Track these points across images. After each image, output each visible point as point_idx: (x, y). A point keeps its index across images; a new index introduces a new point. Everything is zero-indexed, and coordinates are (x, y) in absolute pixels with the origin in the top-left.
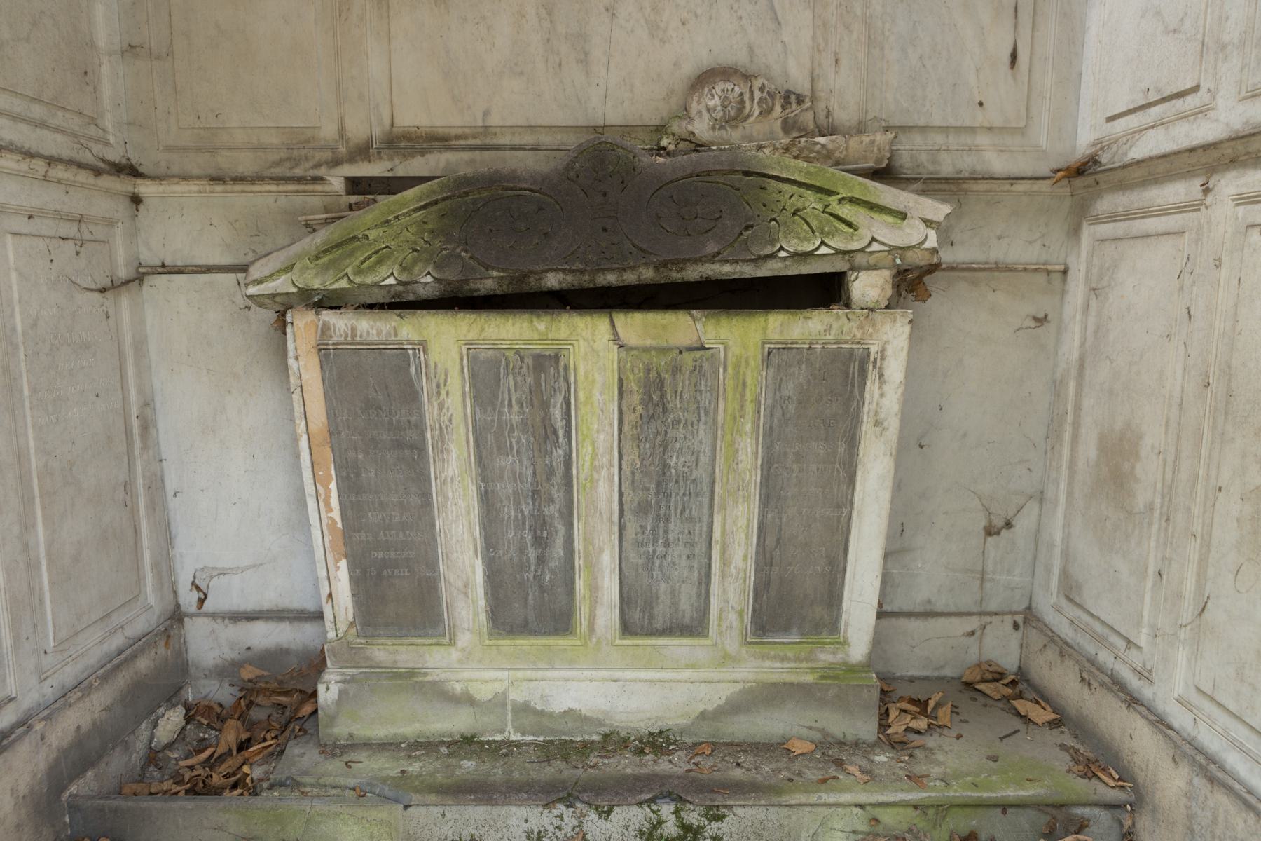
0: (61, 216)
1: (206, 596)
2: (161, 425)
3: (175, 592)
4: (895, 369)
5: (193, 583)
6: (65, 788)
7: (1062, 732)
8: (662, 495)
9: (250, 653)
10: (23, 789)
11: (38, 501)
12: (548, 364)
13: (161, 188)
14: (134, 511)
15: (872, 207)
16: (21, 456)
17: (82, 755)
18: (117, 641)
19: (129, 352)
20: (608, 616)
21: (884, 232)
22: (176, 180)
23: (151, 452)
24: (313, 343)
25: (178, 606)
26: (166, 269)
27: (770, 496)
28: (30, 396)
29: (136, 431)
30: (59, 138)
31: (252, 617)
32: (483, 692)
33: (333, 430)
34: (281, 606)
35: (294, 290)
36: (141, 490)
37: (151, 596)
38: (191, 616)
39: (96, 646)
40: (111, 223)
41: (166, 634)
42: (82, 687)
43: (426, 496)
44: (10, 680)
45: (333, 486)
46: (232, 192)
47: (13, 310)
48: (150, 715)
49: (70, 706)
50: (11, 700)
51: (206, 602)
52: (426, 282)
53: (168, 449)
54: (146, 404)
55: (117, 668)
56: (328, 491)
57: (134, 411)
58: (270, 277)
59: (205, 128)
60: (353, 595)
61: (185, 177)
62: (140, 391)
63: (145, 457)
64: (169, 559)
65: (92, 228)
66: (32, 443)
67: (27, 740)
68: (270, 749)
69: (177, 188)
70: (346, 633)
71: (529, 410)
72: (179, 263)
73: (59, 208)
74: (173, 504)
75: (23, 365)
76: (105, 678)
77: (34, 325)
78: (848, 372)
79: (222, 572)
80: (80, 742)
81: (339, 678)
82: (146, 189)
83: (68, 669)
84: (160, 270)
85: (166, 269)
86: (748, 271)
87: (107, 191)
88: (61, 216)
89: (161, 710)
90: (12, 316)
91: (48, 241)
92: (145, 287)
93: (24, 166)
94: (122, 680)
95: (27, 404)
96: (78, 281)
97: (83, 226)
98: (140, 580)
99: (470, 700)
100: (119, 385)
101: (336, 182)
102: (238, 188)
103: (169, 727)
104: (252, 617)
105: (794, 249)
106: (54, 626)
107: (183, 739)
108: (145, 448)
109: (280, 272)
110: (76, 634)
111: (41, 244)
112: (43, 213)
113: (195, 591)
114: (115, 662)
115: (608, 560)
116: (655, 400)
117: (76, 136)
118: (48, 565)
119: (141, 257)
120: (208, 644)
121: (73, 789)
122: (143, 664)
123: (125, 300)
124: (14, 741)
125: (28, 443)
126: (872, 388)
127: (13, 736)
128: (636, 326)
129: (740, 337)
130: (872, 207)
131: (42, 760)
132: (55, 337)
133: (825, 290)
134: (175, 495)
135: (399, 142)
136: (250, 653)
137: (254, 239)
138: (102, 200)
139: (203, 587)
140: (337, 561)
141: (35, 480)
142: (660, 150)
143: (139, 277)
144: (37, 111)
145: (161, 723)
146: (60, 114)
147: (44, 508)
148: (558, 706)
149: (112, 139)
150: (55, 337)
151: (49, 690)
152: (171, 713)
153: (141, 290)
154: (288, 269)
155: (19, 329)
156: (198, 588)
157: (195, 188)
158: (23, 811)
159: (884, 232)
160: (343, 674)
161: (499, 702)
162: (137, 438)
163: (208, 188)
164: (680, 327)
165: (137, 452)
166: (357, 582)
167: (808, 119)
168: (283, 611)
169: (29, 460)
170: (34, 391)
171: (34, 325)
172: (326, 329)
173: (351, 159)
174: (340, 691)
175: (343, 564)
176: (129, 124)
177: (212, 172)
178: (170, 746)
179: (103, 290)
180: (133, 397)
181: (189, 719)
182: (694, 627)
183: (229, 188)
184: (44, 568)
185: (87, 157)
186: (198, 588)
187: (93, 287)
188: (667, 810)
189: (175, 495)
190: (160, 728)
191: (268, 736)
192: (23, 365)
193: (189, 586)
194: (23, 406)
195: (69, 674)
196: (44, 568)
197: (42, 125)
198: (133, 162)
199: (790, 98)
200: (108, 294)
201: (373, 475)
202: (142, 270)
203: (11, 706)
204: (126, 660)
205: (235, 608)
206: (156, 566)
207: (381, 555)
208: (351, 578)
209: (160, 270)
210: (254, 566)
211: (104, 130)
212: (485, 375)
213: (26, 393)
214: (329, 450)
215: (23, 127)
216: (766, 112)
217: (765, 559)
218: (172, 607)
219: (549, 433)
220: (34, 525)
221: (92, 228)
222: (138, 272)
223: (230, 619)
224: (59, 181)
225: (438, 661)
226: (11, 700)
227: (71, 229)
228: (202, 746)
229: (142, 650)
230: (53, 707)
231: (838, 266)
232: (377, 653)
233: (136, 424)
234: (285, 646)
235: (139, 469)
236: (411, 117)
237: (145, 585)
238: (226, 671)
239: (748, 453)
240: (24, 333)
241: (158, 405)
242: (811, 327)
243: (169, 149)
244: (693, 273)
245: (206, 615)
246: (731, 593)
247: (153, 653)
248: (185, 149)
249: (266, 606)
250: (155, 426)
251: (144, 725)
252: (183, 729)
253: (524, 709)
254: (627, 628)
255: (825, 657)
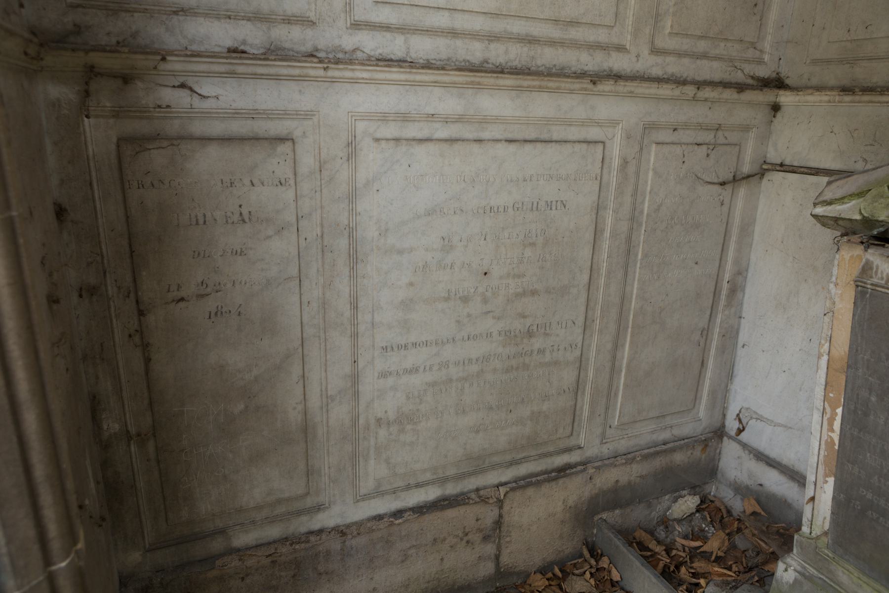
0: (701, 127)
1: (744, 429)
2: (747, 291)
3: (724, 416)
5: (738, 415)
6: (598, 513)
9: (760, 488)
10: (571, 502)
11: (630, 330)
13: (797, 98)
14: (705, 350)
16: (624, 298)
17: (615, 498)
18: (666, 435)
19: (735, 231)
22: (810, 91)
23: (733, 310)
24: (854, 276)
25: (723, 426)
26: (783, 167)
28: (642, 259)
29: (724, 292)
30: (716, 64)
31: (772, 463)
33: (852, 363)
34: (797, 468)
35: (858, 217)
36: (716, 336)
37: (702, 411)
38: (730, 437)
39: (646, 434)
40: (746, 129)
41: (705, 443)
42: (628, 457)
44: (582, 436)
45: (839, 411)
46: (859, 102)
47: (645, 198)
48: (676, 491)
49: (615, 466)
50: (580, 448)
51: (743, 434)
53: (748, 311)
54: (739, 273)
55: (657, 453)
56: (834, 414)
57: (727, 277)
58: (841, 200)
59: (851, 41)
60: (832, 513)
61: (819, 88)
62: (737, 262)
63: (727, 312)
64: (727, 390)
65: (726, 134)
66: (635, 292)
67: (581, 475)
68: (730, 579)
69: (810, 98)
70: (818, 538)
72: (796, 164)
73: (701, 120)
74: (740, 352)
75: (642, 237)
76: (646, 457)
77: (658, 210)
79: (760, 418)
80: (616, 489)
81: (799, 568)
82: (785, 98)
83: (623, 442)
84: (778, 168)
85: (783, 167)
87: (750, 104)
88: (701, 127)
89: (685, 492)
90: (643, 202)
91: (684, 147)
92: (765, 181)
93: (677, 92)
94: (658, 463)
95: (638, 265)
96: (703, 177)
97: (720, 133)
98: (696, 399)
100: (718, 257)
102: (866, 98)
103: (683, 507)
104: (772, 463)
106: (620, 413)
107: (691, 521)
108: (729, 305)
109: (852, 196)
110: (635, 422)
111: (678, 150)
112: (686, 126)
113: (737, 422)
114: (658, 449)
117: (731, 60)
118: (626, 373)
119: (768, 155)
120: (734, 464)
121: (604, 516)
122: (679, 458)
123: (742, 191)
124: (573, 474)
125: (632, 291)
127: (574, 470)
131: (587, 491)
132: (672, 219)
134: (743, 346)
136: (760, 488)
137: (869, 148)
138: (746, 110)
139: (744, 421)
140: (826, 476)
141: (631, 317)
143: (762, 171)
144: (702, 46)
145: (680, 501)
146: (722, 44)
147: (632, 336)
149: (766, 58)
150: (672, 219)
151: (606, 450)
152: (690, 498)
153: (760, 183)
154: (860, 194)
155: (646, 212)
156: (740, 421)
157: (826, 98)
158: (568, 515)
160: (804, 568)
162: (723, 297)
163: (837, 98)
165: (721, 308)
166: (840, 504)
168: (797, 473)
169: (631, 302)
170: (645, 256)
171: (658, 210)
172: (867, 269)
174: (796, 580)
175: (831, 480)
176: (788, 42)
177: (846, 82)
178: (679, 521)
179: (723, 184)
180: (729, 267)
181: (699, 510)
183: (857, 98)
184: (623, 374)
185: (739, 77)
186: (740, 421)
187: (716, 181)
189: (743, 346)
190: (677, 504)
191: (734, 568)
192: (642, 237)
193: (735, 416)
194: (635, 266)
195: (623, 445)
196: (623, 374)
197: (704, 56)
198: (782, 75)
200: (726, 186)
201: (882, 422)
202: (765, 167)
203: (579, 451)
204: (665, 451)
205: (761, 449)
206: (713, 393)
207: (869, 496)
208: (834, 498)
209: (778, 168)
210: (785, 427)
211: (761, 51)
213: (640, 256)
214: (844, 377)
215: (686, 61)
218: (719, 425)
220: (623, 346)
221: (726, 134)
222: (761, 168)
223: (755, 455)
224: (706, 100)
226: (580, 448)
227: (708, 137)
228: (700, 535)
229: (681, 448)
230: (606, 462)
232: (840, 574)
233: (725, 286)
234: (790, 501)
235: (718, 320)
237: (700, 404)
238: (741, 490)
240: (648, 215)
241: (750, 275)
243: (815, 62)
245: (740, 443)
247: (689, 453)
248: (828, 62)
249: (785, 461)
250: (743, 291)
251: (667, 497)
252: (692, 514)
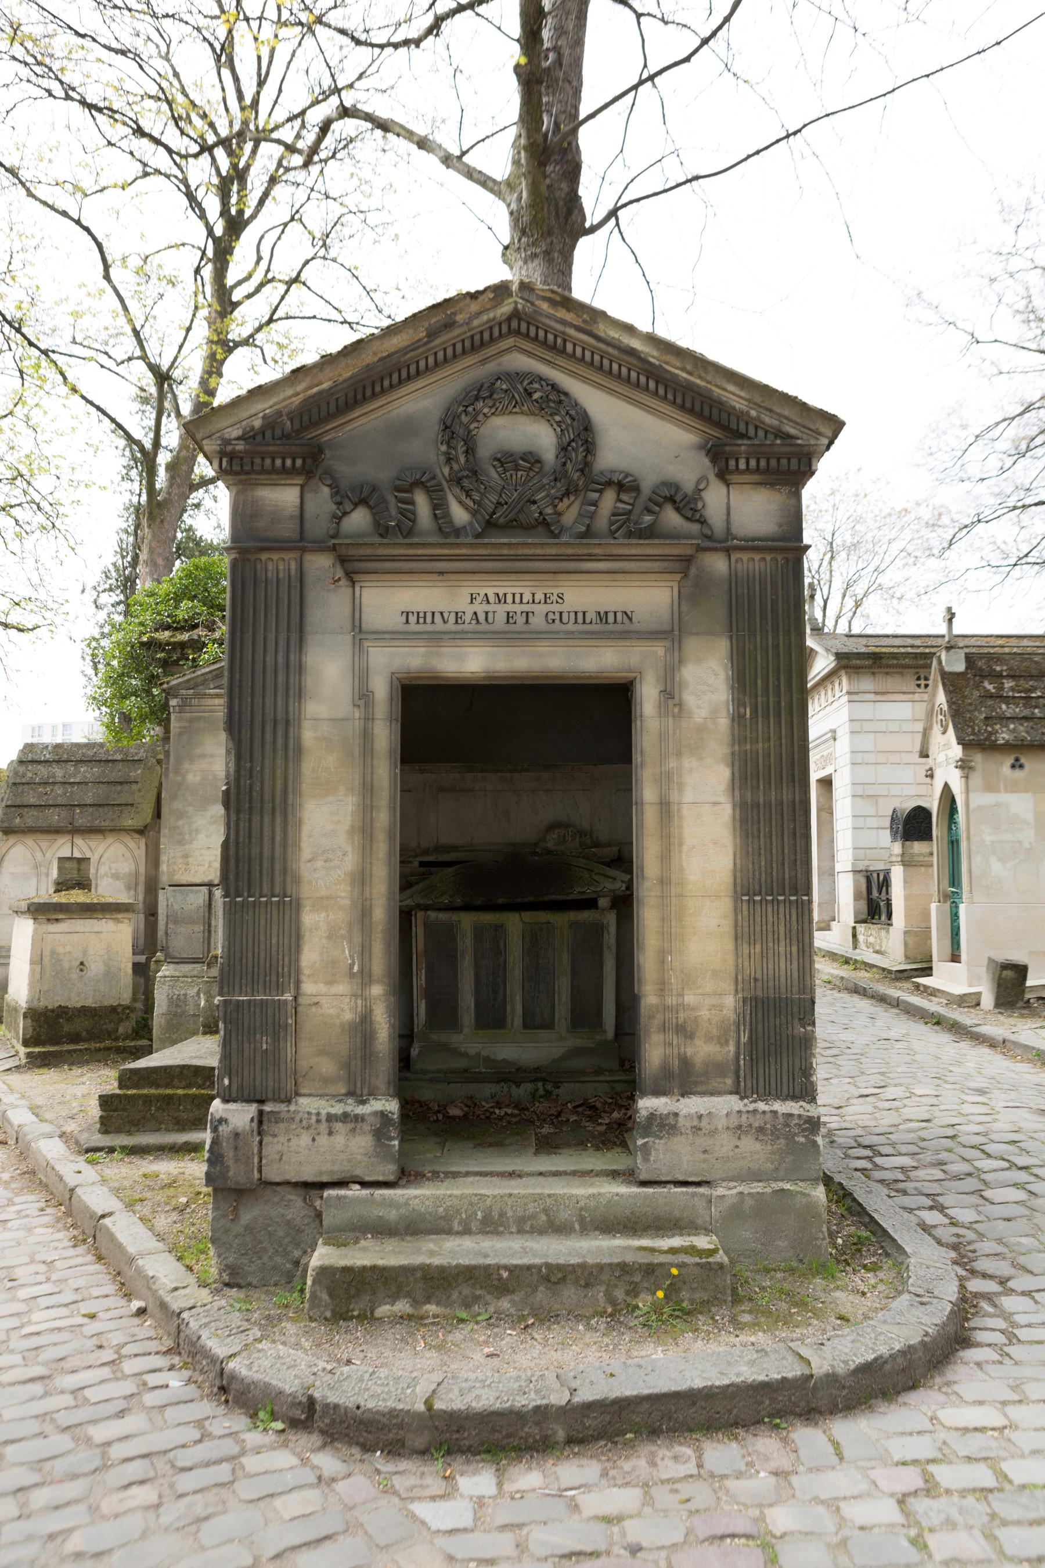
4: (613, 929)
7: (197, 506)
8: (537, 975)
12: (499, 929)
15: (606, 876)
20: (518, 1021)
21: (609, 885)
27: (574, 974)
32: (472, 1052)
43: (456, 974)
52: (459, 901)
71: (491, 944)
78: (598, 930)
86: (565, 898)
99: (466, 1055)
101: (416, 864)
105: (580, 891)
115: (518, 998)
116: (534, 941)
126: (606, 935)
128: (528, 916)
129: (561, 920)
130: (606, 876)
133: (590, 904)
135: (439, 849)
142: (535, 853)
148: (500, 1057)
159: (609, 885)
161: (478, 1055)
164: (543, 916)
167: (588, 842)
173: (422, 855)
182: (549, 1025)
188: (540, 1084)
199: (582, 833)
212: (479, 932)
216: (574, 839)
217: (574, 998)
219: (499, 952)
225: (456, 1039)
231: (594, 896)
236: (444, 840)
239: (566, 958)
242: (584, 916)
244: (547, 898)
246: (562, 1013)
253: (487, 1059)
254: (525, 1026)
255: (598, 1037)
